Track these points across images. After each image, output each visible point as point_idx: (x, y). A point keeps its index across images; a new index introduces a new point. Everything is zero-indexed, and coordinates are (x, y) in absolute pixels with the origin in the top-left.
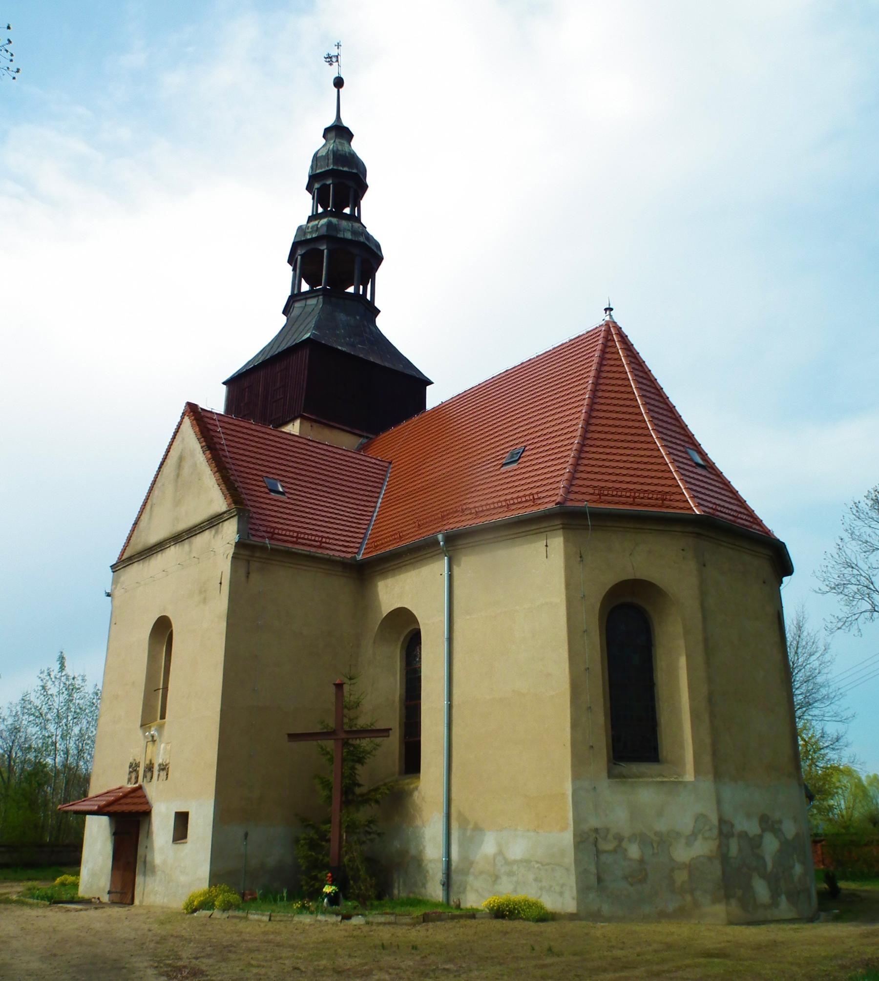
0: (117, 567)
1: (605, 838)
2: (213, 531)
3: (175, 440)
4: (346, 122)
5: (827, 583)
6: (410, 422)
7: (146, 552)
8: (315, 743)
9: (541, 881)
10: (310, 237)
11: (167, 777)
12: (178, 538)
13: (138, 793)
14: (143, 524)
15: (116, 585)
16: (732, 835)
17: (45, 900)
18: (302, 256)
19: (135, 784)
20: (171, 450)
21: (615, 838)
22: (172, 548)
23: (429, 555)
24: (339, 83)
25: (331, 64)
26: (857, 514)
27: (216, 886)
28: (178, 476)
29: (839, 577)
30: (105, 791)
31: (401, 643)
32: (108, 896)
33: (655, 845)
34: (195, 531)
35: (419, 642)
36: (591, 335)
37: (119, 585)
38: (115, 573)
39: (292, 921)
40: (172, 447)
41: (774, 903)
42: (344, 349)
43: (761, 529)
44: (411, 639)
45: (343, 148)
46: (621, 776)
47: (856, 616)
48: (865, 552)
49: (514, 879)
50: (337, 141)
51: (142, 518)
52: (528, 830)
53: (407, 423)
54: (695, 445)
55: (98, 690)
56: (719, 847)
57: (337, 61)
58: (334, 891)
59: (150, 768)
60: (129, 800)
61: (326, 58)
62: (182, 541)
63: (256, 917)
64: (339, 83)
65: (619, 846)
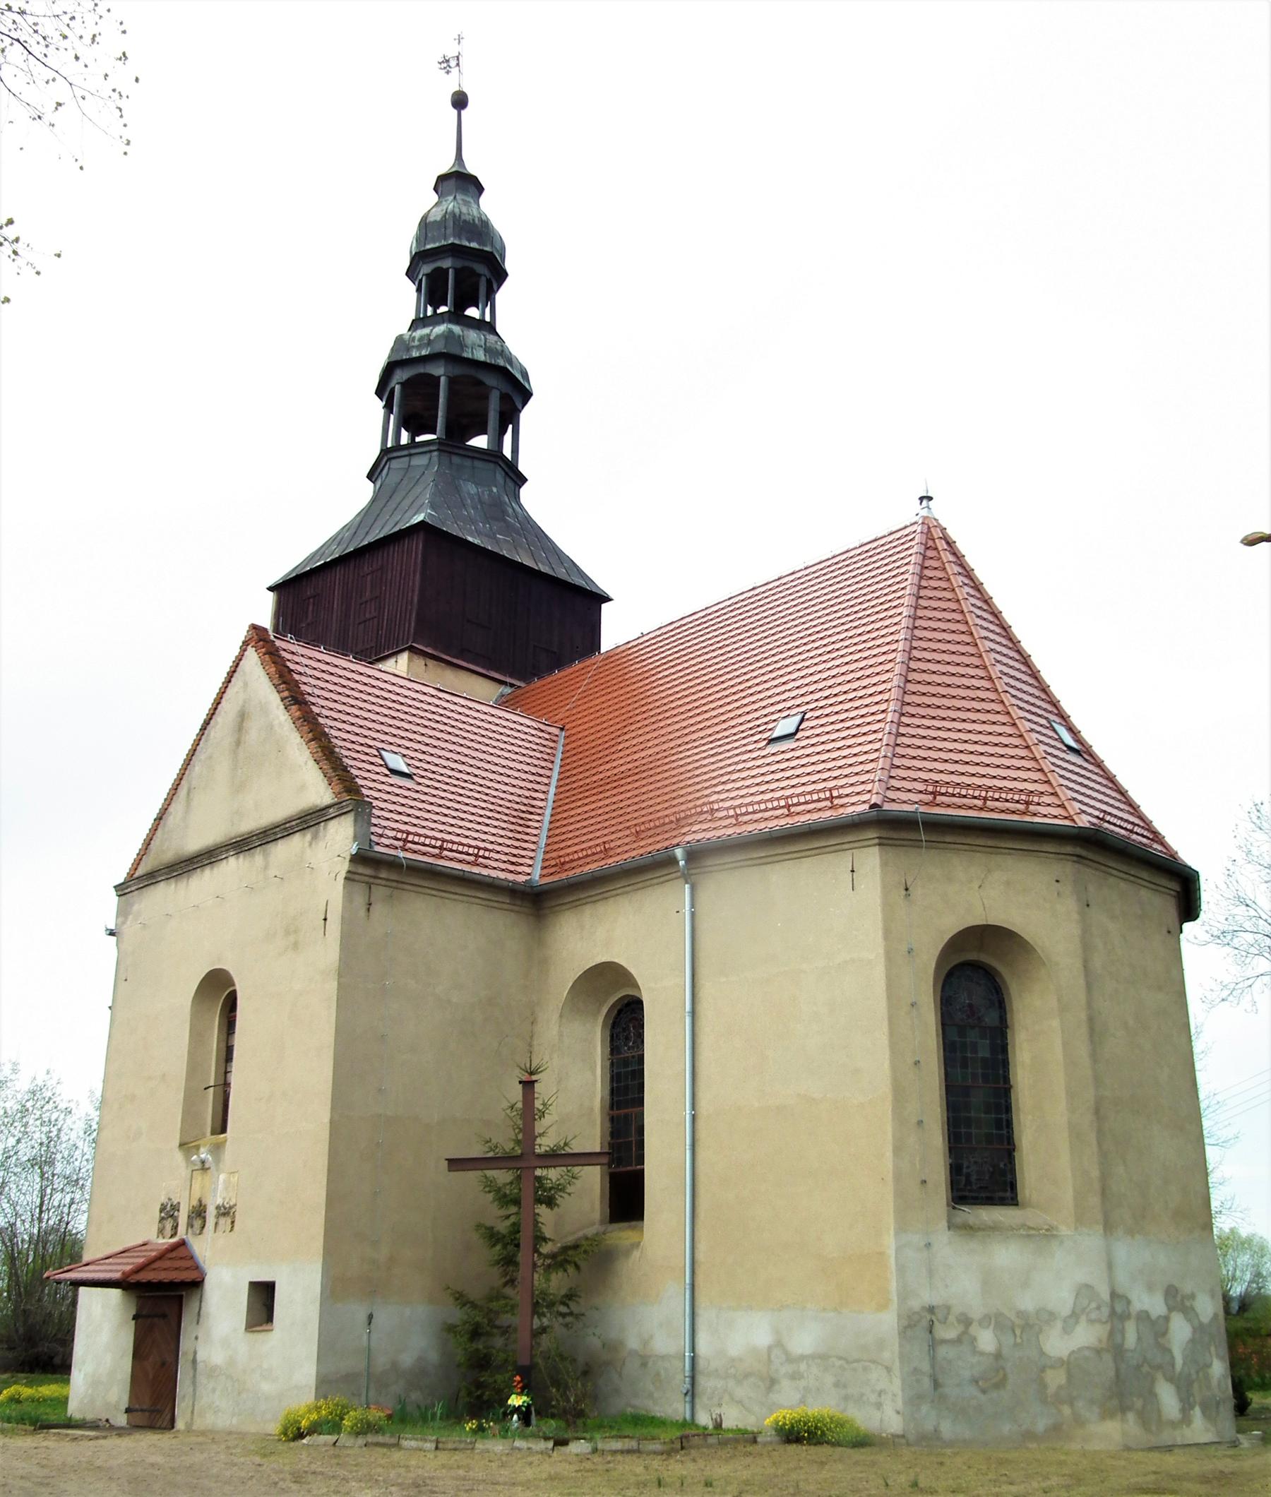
0: (127, 888)
1: (944, 1321)
2: (308, 835)
3: (230, 685)
4: (471, 168)
5: (1208, 928)
6: (587, 663)
7: (182, 865)
8: (480, 1173)
9: (845, 1386)
10: (418, 355)
11: (233, 1227)
12: (243, 845)
13: (181, 1250)
14: (173, 819)
15: (126, 917)
16: (1128, 1317)
17: (25, 1424)
18: (404, 385)
19: (172, 1236)
20: (223, 701)
21: (959, 1321)
22: (232, 860)
23: (655, 881)
24: (460, 101)
25: (448, 72)
26: (1258, 822)
27: (325, 1398)
28: (238, 743)
29: (1226, 919)
30: (120, 1248)
31: (603, 1017)
32: (126, 1416)
33: (1018, 1332)
34: (275, 833)
35: (235, 999)
36: (896, 539)
37: (130, 917)
38: (123, 898)
39: (473, 1449)
40: (226, 696)
41: (1186, 1419)
42: (476, 541)
43: (1165, 851)
44: (620, 1012)
45: (468, 212)
46: (968, 1230)
47: (1250, 982)
48: (1266, 882)
49: (803, 1383)
50: (458, 197)
51: (171, 809)
52: (824, 1309)
53: (581, 666)
54: (1062, 717)
55: (37, 1085)
56: (1111, 1334)
57: (458, 65)
58: (526, 1404)
59: (199, 1212)
60: (167, 1264)
61: (440, 63)
62: (249, 849)
63: (413, 1444)
64: (460, 101)
65: (965, 1332)
